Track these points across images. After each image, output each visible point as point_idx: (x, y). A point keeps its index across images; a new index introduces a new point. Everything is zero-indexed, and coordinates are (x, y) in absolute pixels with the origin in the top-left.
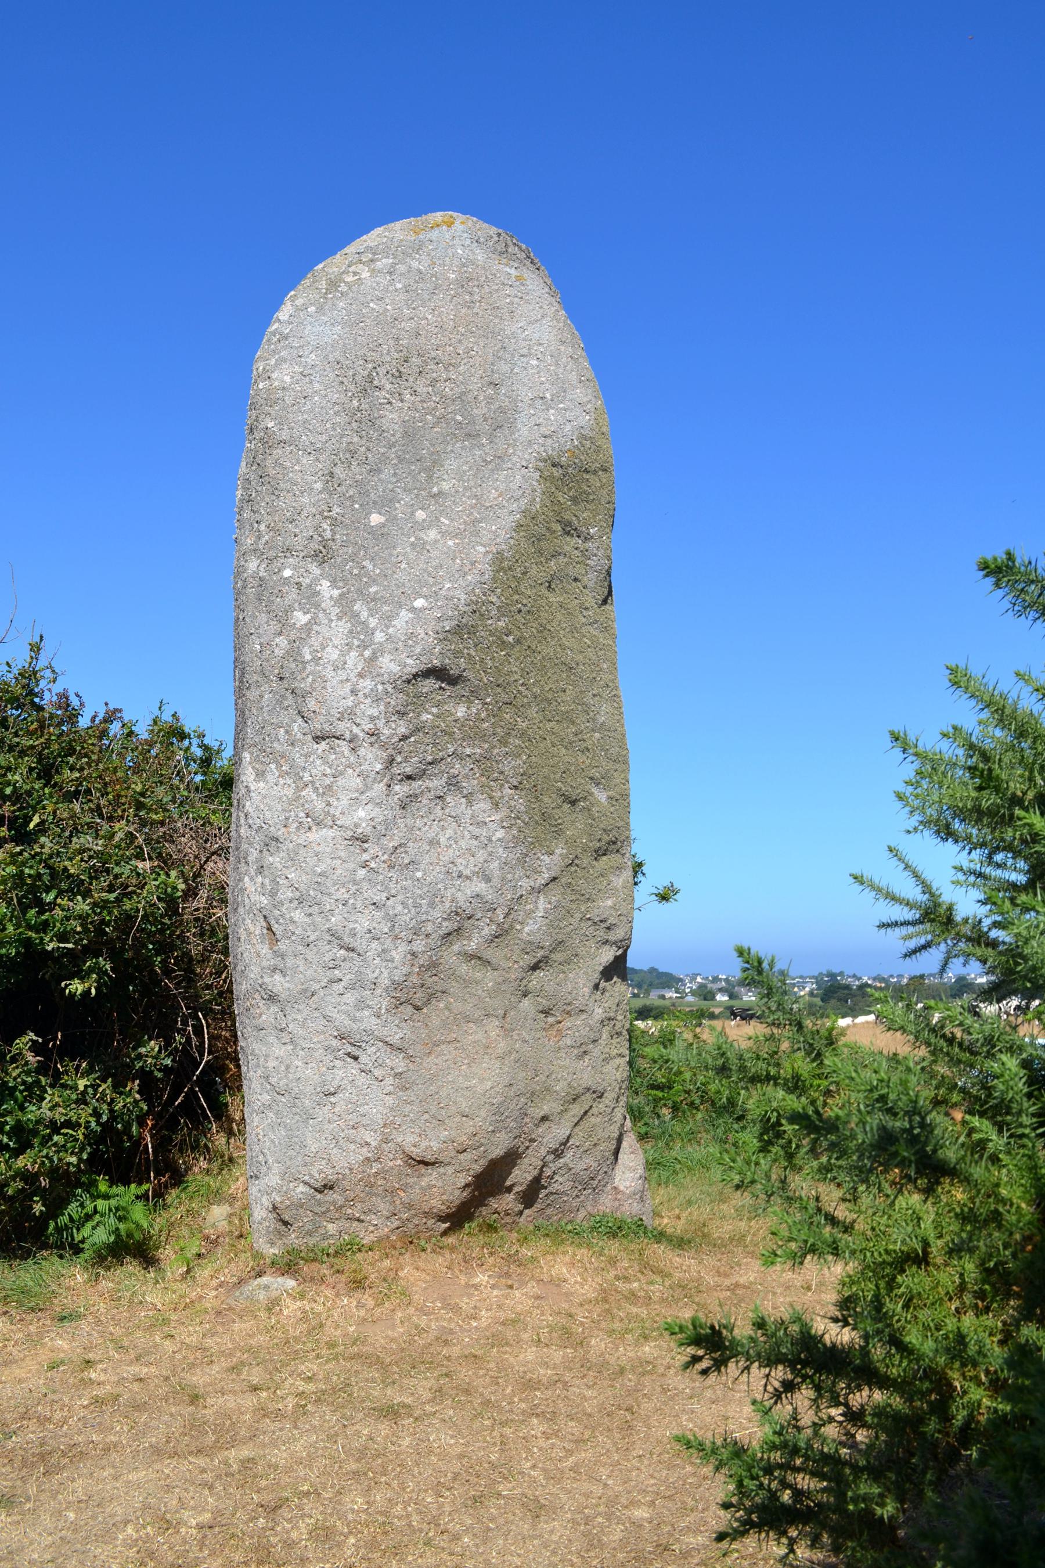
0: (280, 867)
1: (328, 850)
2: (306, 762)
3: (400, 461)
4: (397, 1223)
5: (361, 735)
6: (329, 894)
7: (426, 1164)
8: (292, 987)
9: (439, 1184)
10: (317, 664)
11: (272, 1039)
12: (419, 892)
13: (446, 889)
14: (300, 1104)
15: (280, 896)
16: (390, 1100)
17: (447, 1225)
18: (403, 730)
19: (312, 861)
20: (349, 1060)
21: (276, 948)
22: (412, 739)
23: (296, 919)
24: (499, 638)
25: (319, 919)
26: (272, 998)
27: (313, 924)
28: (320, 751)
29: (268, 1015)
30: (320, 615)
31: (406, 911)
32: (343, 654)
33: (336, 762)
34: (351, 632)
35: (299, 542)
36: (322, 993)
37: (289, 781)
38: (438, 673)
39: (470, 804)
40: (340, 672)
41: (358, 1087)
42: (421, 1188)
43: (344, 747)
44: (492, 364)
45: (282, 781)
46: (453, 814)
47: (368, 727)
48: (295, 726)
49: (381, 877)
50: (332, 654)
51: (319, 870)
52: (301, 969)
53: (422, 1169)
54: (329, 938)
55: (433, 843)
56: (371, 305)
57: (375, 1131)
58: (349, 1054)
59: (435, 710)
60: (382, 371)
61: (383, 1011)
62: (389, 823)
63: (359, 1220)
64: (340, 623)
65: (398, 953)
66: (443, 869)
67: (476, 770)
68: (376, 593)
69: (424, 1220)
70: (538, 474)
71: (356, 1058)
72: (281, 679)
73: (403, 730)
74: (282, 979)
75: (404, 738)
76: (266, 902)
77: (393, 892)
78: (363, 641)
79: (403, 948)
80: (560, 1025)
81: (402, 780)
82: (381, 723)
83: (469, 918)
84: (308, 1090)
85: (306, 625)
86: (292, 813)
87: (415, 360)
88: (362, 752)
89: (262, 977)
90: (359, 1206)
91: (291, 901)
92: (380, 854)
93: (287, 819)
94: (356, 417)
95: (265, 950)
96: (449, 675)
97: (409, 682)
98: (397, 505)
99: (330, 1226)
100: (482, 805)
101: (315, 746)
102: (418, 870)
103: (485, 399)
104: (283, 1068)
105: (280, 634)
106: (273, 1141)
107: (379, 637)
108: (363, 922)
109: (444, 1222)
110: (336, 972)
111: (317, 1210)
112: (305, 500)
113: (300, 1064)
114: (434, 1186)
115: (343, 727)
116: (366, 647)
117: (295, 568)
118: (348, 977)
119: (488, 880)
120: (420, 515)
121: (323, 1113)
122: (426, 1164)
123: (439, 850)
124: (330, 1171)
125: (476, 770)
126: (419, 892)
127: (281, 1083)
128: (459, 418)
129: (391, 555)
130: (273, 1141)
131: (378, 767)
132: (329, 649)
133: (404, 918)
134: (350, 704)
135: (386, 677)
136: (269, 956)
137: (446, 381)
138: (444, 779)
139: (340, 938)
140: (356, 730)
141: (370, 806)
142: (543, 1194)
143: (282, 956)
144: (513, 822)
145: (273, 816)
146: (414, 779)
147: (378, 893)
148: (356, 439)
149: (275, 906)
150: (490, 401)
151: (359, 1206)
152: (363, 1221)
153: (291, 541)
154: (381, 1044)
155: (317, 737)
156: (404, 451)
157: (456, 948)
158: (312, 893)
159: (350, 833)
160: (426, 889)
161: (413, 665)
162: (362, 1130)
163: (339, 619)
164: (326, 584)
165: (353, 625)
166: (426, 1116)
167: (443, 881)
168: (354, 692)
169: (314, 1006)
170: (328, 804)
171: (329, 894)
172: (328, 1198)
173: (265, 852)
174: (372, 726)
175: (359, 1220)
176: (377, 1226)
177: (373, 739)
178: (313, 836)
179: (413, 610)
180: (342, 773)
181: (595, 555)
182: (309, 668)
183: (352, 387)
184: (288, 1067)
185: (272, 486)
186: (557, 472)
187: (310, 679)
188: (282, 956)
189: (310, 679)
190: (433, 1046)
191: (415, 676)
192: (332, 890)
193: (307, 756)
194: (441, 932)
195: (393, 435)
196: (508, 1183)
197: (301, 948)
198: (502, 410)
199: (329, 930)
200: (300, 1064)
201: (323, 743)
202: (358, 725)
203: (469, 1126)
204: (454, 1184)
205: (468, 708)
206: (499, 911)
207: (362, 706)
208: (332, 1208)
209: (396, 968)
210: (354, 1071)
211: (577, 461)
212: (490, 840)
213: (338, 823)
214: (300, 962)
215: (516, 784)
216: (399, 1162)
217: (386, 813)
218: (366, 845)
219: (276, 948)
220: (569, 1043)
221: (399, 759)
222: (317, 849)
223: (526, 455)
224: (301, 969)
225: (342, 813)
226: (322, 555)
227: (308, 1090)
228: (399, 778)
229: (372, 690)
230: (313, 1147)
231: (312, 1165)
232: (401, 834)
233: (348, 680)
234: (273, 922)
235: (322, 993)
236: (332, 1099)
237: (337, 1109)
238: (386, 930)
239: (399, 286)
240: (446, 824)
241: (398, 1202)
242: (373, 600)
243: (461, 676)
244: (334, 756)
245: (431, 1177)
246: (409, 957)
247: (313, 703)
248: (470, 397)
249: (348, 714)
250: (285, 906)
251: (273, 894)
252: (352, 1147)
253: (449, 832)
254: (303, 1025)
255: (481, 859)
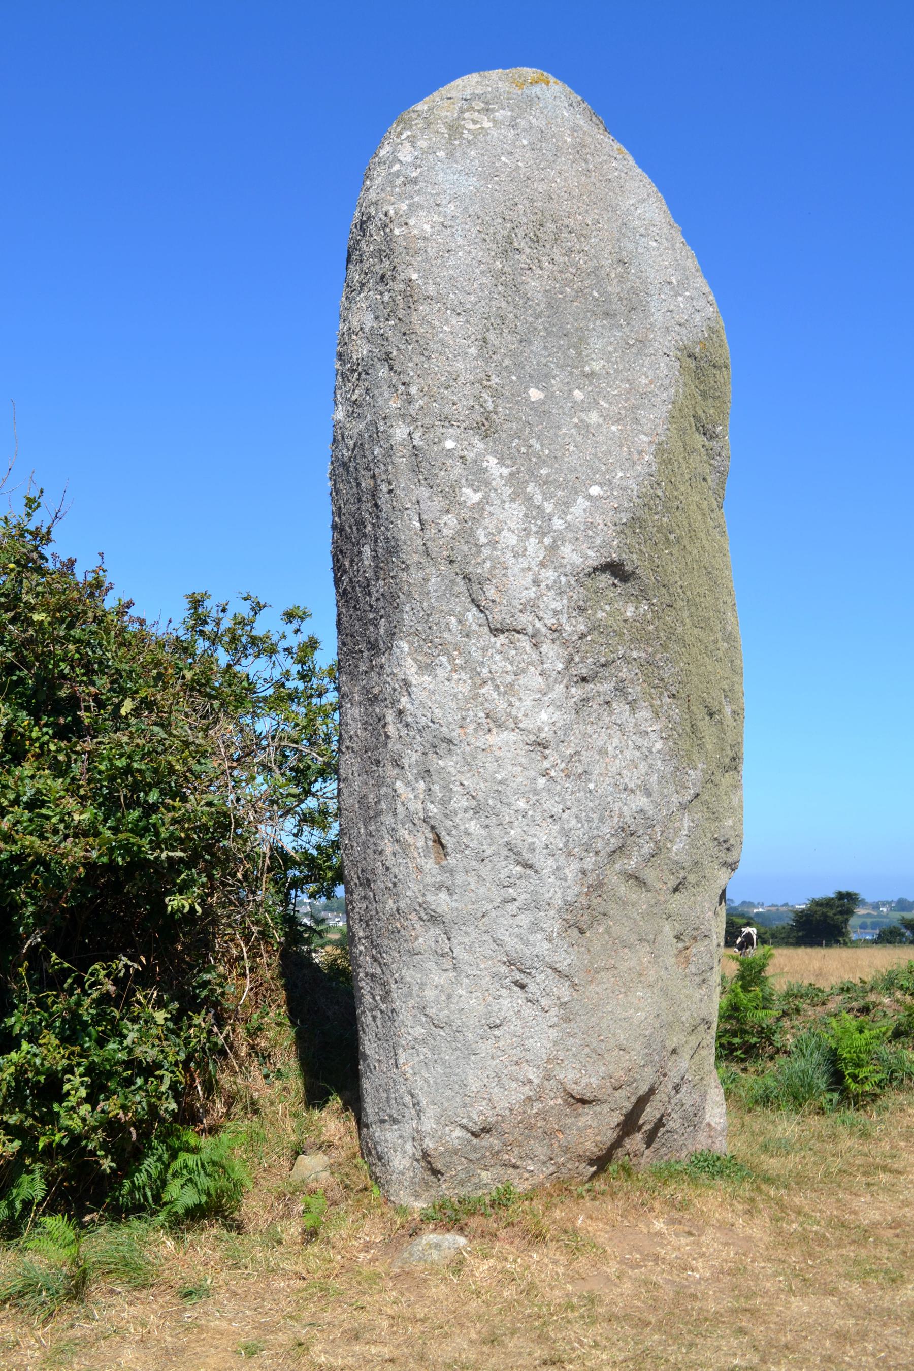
0: (454, 772)
1: (509, 755)
2: (484, 656)
3: (549, 333)
4: (552, 1169)
5: (544, 630)
6: (509, 805)
7: (583, 1102)
8: (460, 906)
9: (595, 1124)
10: (495, 549)
11: (431, 965)
12: (591, 805)
13: (614, 802)
14: (461, 1038)
15: (453, 805)
16: (553, 1033)
17: (594, 1169)
18: (582, 628)
19: (491, 767)
20: (516, 988)
21: (444, 863)
22: (589, 638)
23: (471, 830)
24: (665, 536)
25: (497, 832)
26: (434, 918)
27: (490, 836)
28: (498, 645)
29: (426, 938)
30: (492, 495)
31: (580, 825)
32: (521, 540)
33: (517, 658)
34: (526, 516)
35: (461, 410)
36: (493, 913)
37: (464, 676)
38: (615, 569)
39: (633, 710)
40: (521, 559)
41: (524, 1018)
42: (579, 1129)
43: (524, 642)
44: (618, 240)
45: (455, 676)
46: (618, 721)
47: (550, 622)
48: (470, 616)
49: (558, 787)
50: (510, 539)
51: (499, 777)
52: (473, 886)
53: (580, 1108)
54: (506, 853)
55: (603, 752)
56: (503, 159)
57: (538, 1067)
58: (516, 983)
59: (607, 608)
60: (520, 232)
61: (555, 935)
62: (567, 729)
63: (515, 1167)
64: (514, 506)
65: (571, 871)
66: (612, 781)
67: (640, 675)
68: (548, 475)
69: (577, 1164)
70: (678, 364)
71: (522, 987)
72: (451, 562)
73: (583, 627)
74: (448, 898)
75: (582, 636)
76: (435, 811)
77: (569, 804)
78: (540, 527)
79: (575, 866)
80: (687, 951)
81: (577, 682)
82: (563, 619)
83: (632, 835)
84: (472, 1022)
85: (478, 504)
86: (471, 713)
87: (550, 226)
88: (544, 648)
89: (424, 895)
90: (516, 1150)
91: (465, 811)
92: (559, 761)
93: (464, 718)
94: (501, 280)
95: (429, 864)
96: (623, 571)
97: (589, 575)
98: (553, 382)
99: (484, 1174)
100: (644, 713)
101: (493, 639)
102: (590, 781)
103: (616, 277)
104: (444, 998)
105: (448, 512)
106: (426, 1080)
107: (558, 524)
108: (543, 835)
109: (592, 1166)
110: (511, 890)
111: (473, 1156)
112: (460, 365)
113: (463, 993)
114: (590, 1126)
115: (524, 620)
116: (544, 534)
117: (457, 439)
118: (523, 896)
119: (649, 794)
120: (578, 395)
121: (485, 1047)
122: (583, 1102)
123: (607, 760)
124: (489, 1113)
125: (640, 675)
126: (591, 805)
127: (442, 1015)
128: (596, 294)
129: (557, 436)
130: (426, 1080)
131: (560, 666)
132: (505, 533)
133: (580, 832)
134: (533, 595)
135: (568, 569)
136: (435, 871)
137: (579, 253)
138: (613, 684)
139: (518, 854)
140: (538, 624)
141: (551, 709)
142: (662, 1130)
143: (452, 872)
144: (670, 733)
145: (446, 716)
146: (587, 682)
147: (556, 805)
148: (504, 304)
149: (446, 816)
150: (622, 279)
151: (516, 1150)
152: (518, 1168)
153: (449, 409)
154: (550, 971)
155: (496, 630)
156: (549, 323)
157: (618, 866)
158: (490, 802)
159: (532, 738)
160: (597, 802)
161: (594, 558)
162: (525, 1066)
163: (513, 500)
164: (493, 461)
165: (528, 509)
166: (587, 1050)
167: (611, 794)
168: (536, 582)
169: (483, 928)
170: (511, 705)
171: (509, 805)
172: (484, 1143)
173: (431, 755)
174: (555, 621)
175: (515, 1167)
176: (535, 1172)
177: (556, 635)
178: (494, 739)
179: (589, 497)
180: (524, 671)
181: (719, 455)
182: (486, 552)
183: (494, 246)
184: (449, 997)
185: (420, 346)
186: (692, 364)
187: (488, 564)
188: (452, 872)
189: (488, 564)
190: (593, 973)
191: (595, 569)
192: (513, 799)
193: (484, 650)
194: (608, 850)
195: (538, 304)
196: (641, 1122)
197: (474, 863)
198: (634, 291)
199: (508, 843)
200: (463, 993)
201: (502, 636)
202: (540, 619)
203: (626, 1060)
204: (608, 1124)
205: (636, 608)
206: (658, 829)
207: (545, 598)
208: (488, 1154)
209: (569, 887)
210: (520, 1002)
211: (708, 354)
212: (651, 752)
213: (521, 725)
214: (472, 880)
215: (675, 692)
216: (560, 1101)
217: (565, 717)
218: (547, 752)
219: (444, 863)
220: (694, 970)
221: (577, 659)
222: (497, 753)
223: (663, 342)
224: (473, 886)
225: (526, 715)
226: (485, 427)
227: (472, 1022)
228: (575, 679)
229: (555, 582)
230: (474, 1086)
231: (472, 1106)
232: (577, 741)
233: (529, 569)
234: (443, 834)
235: (493, 913)
236: (497, 1032)
237: (501, 1044)
238: (561, 846)
239: (525, 142)
240: (612, 732)
241: (556, 1145)
242: (545, 483)
243: (634, 573)
244: (514, 652)
245: (587, 1117)
246: (580, 876)
247: (492, 591)
248: (603, 273)
249: (531, 606)
250: (460, 816)
251: (444, 803)
252: (514, 1085)
253: (616, 742)
254: (470, 949)
255: (643, 771)
